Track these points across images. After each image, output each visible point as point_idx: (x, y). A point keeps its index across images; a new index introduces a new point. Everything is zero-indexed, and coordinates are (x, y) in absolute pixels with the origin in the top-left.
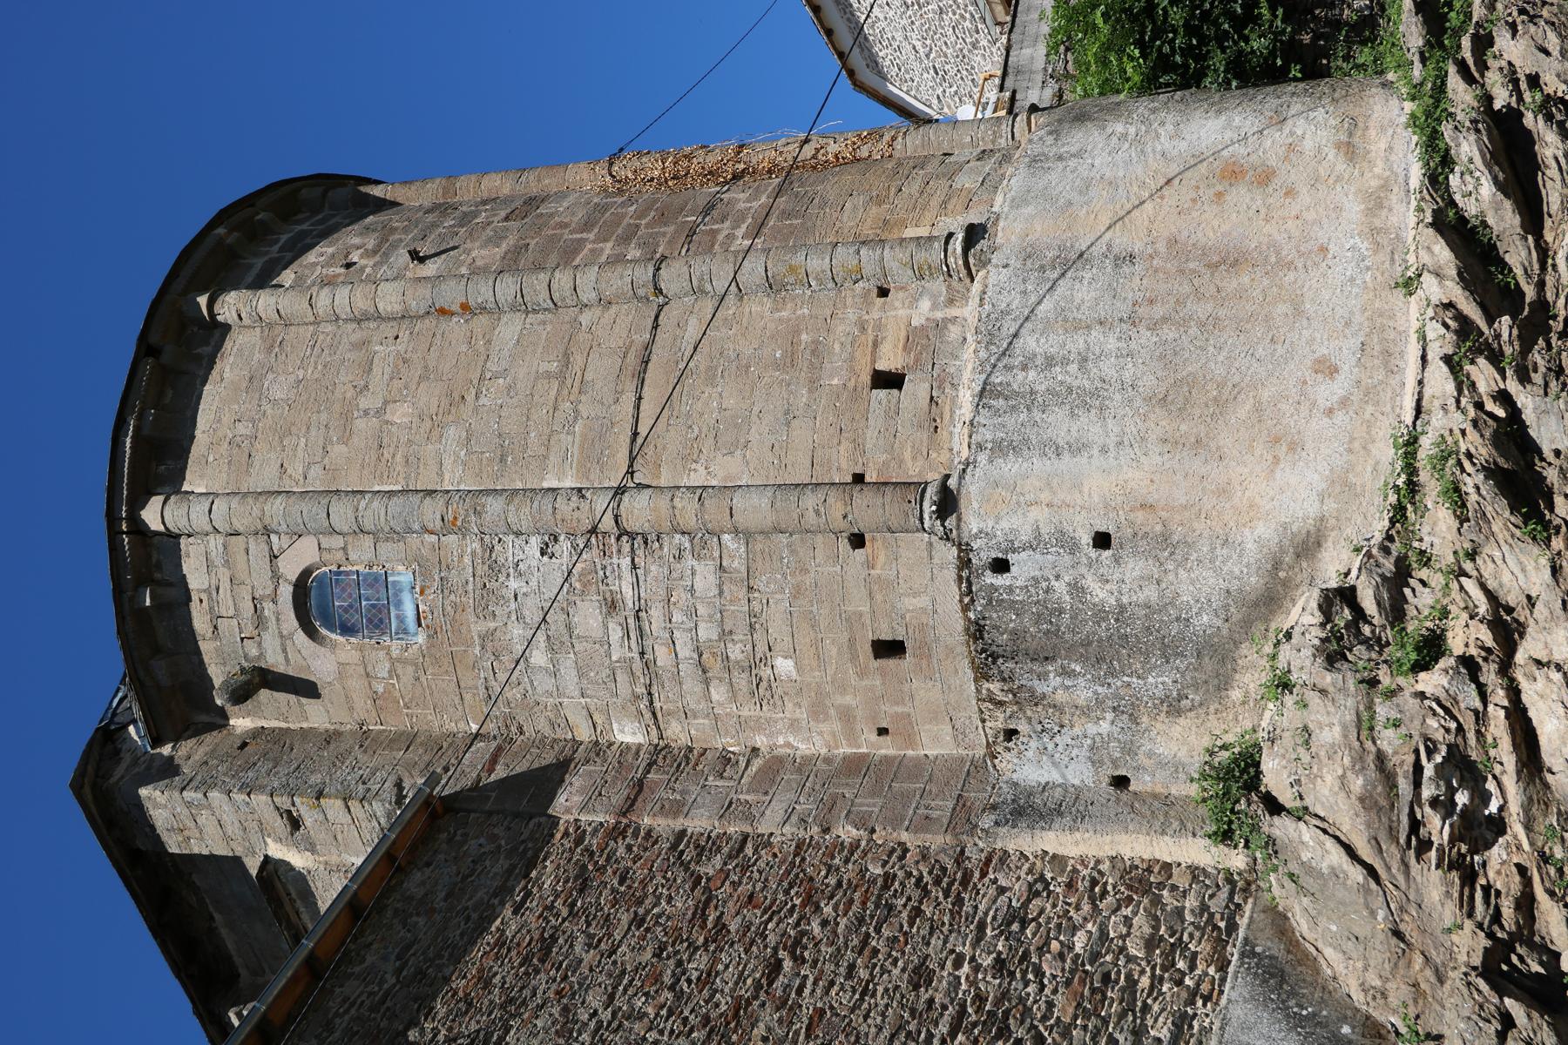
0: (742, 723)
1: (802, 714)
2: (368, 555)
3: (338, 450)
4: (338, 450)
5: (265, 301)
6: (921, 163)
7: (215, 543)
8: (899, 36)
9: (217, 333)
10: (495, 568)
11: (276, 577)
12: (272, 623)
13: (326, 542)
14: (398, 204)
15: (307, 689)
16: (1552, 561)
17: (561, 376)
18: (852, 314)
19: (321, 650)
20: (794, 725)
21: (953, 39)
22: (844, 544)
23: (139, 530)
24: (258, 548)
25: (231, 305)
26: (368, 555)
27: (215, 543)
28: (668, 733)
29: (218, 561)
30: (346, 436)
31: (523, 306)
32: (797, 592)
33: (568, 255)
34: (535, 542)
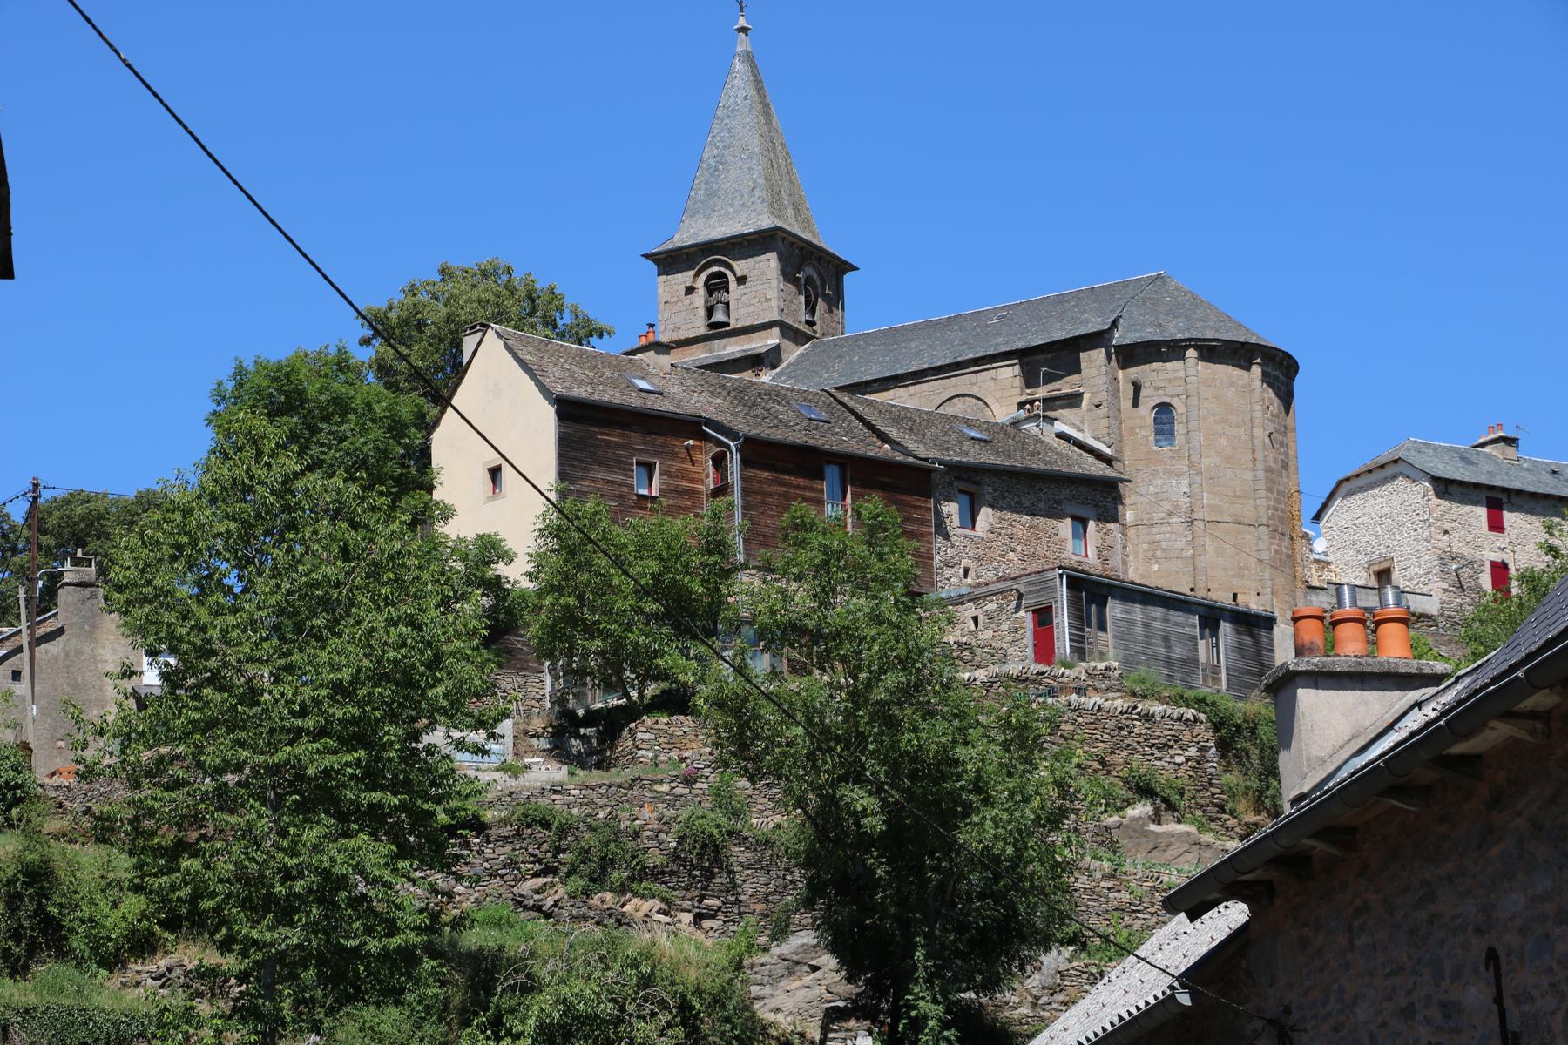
0: (1136, 553)
1: (1141, 572)
2: (1181, 432)
3: (1212, 419)
4: (1212, 419)
5: (1257, 383)
6: (1294, 599)
7: (1182, 374)
8: (1366, 510)
9: (1247, 364)
10: (1178, 475)
11: (1172, 396)
12: (1157, 393)
13: (1184, 416)
14: (1287, 413)
15: (1136, 404)
16: (1429, 617)
17: (1235, 496)
18: (1253, 586)
19: (1149, 411)
20: (1137, 569)
21: (1363, 540)
22: (1191, 586)
23: (1187, 348)
24: (1180, 390)
25: (1257, 370)
26: (1181, 432)
27: (1182, 374)
28: (1131, 529)
29: (1176, 375)
30: (1218, 422)
31: (1255, 479)
32: (1177, 572)
33: (1270, 490)
34: (1187, 490)
